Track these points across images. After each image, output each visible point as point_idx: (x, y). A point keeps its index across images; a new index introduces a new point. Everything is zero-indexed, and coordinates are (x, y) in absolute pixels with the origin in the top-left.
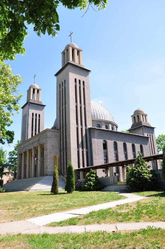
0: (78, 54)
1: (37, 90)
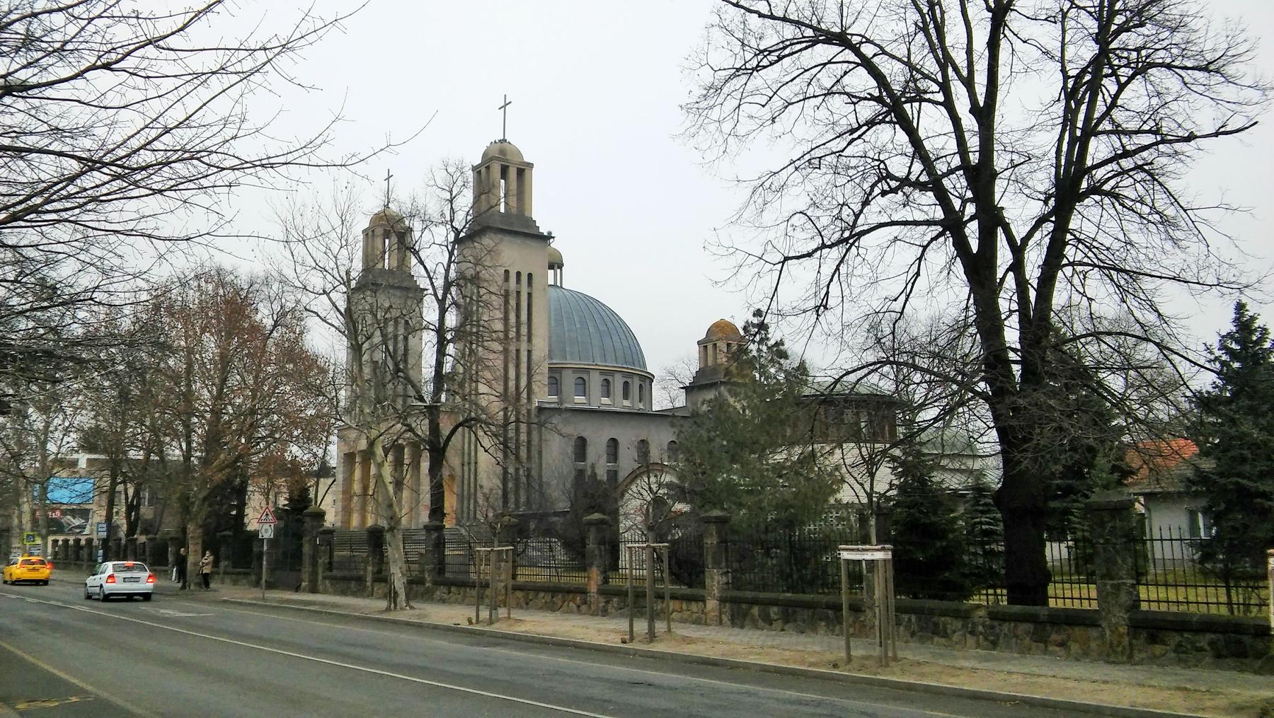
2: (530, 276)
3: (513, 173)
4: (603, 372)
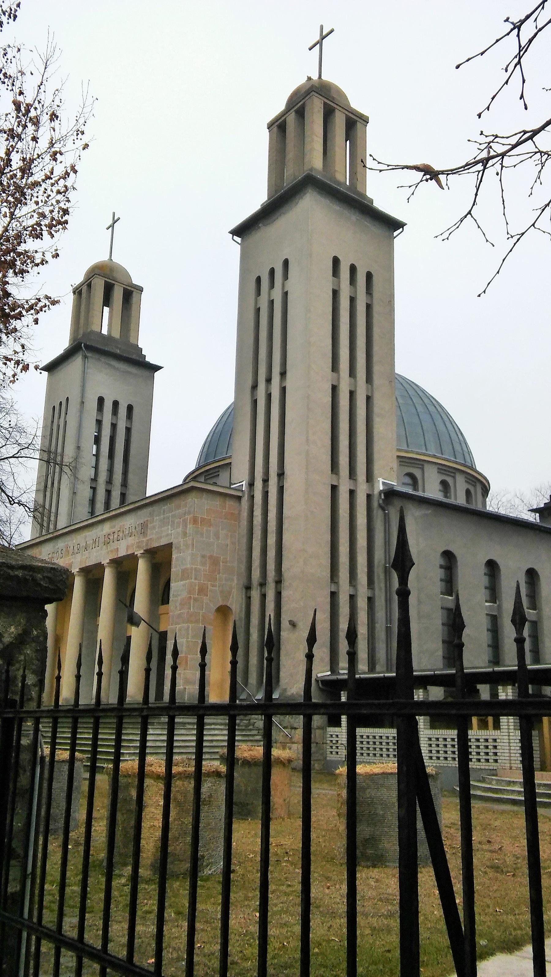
0: (348, 137)
1: (125, 289)
2: (130, 408)
3: (118, 295)
4: (443, 469)
